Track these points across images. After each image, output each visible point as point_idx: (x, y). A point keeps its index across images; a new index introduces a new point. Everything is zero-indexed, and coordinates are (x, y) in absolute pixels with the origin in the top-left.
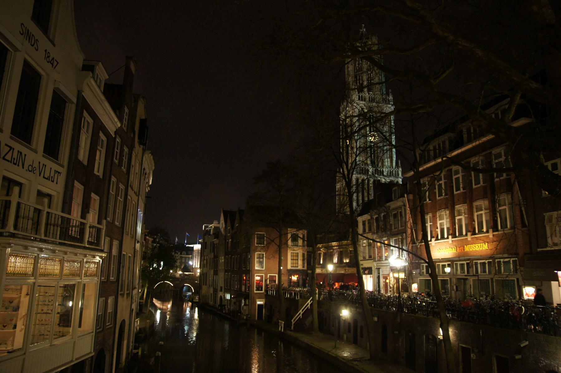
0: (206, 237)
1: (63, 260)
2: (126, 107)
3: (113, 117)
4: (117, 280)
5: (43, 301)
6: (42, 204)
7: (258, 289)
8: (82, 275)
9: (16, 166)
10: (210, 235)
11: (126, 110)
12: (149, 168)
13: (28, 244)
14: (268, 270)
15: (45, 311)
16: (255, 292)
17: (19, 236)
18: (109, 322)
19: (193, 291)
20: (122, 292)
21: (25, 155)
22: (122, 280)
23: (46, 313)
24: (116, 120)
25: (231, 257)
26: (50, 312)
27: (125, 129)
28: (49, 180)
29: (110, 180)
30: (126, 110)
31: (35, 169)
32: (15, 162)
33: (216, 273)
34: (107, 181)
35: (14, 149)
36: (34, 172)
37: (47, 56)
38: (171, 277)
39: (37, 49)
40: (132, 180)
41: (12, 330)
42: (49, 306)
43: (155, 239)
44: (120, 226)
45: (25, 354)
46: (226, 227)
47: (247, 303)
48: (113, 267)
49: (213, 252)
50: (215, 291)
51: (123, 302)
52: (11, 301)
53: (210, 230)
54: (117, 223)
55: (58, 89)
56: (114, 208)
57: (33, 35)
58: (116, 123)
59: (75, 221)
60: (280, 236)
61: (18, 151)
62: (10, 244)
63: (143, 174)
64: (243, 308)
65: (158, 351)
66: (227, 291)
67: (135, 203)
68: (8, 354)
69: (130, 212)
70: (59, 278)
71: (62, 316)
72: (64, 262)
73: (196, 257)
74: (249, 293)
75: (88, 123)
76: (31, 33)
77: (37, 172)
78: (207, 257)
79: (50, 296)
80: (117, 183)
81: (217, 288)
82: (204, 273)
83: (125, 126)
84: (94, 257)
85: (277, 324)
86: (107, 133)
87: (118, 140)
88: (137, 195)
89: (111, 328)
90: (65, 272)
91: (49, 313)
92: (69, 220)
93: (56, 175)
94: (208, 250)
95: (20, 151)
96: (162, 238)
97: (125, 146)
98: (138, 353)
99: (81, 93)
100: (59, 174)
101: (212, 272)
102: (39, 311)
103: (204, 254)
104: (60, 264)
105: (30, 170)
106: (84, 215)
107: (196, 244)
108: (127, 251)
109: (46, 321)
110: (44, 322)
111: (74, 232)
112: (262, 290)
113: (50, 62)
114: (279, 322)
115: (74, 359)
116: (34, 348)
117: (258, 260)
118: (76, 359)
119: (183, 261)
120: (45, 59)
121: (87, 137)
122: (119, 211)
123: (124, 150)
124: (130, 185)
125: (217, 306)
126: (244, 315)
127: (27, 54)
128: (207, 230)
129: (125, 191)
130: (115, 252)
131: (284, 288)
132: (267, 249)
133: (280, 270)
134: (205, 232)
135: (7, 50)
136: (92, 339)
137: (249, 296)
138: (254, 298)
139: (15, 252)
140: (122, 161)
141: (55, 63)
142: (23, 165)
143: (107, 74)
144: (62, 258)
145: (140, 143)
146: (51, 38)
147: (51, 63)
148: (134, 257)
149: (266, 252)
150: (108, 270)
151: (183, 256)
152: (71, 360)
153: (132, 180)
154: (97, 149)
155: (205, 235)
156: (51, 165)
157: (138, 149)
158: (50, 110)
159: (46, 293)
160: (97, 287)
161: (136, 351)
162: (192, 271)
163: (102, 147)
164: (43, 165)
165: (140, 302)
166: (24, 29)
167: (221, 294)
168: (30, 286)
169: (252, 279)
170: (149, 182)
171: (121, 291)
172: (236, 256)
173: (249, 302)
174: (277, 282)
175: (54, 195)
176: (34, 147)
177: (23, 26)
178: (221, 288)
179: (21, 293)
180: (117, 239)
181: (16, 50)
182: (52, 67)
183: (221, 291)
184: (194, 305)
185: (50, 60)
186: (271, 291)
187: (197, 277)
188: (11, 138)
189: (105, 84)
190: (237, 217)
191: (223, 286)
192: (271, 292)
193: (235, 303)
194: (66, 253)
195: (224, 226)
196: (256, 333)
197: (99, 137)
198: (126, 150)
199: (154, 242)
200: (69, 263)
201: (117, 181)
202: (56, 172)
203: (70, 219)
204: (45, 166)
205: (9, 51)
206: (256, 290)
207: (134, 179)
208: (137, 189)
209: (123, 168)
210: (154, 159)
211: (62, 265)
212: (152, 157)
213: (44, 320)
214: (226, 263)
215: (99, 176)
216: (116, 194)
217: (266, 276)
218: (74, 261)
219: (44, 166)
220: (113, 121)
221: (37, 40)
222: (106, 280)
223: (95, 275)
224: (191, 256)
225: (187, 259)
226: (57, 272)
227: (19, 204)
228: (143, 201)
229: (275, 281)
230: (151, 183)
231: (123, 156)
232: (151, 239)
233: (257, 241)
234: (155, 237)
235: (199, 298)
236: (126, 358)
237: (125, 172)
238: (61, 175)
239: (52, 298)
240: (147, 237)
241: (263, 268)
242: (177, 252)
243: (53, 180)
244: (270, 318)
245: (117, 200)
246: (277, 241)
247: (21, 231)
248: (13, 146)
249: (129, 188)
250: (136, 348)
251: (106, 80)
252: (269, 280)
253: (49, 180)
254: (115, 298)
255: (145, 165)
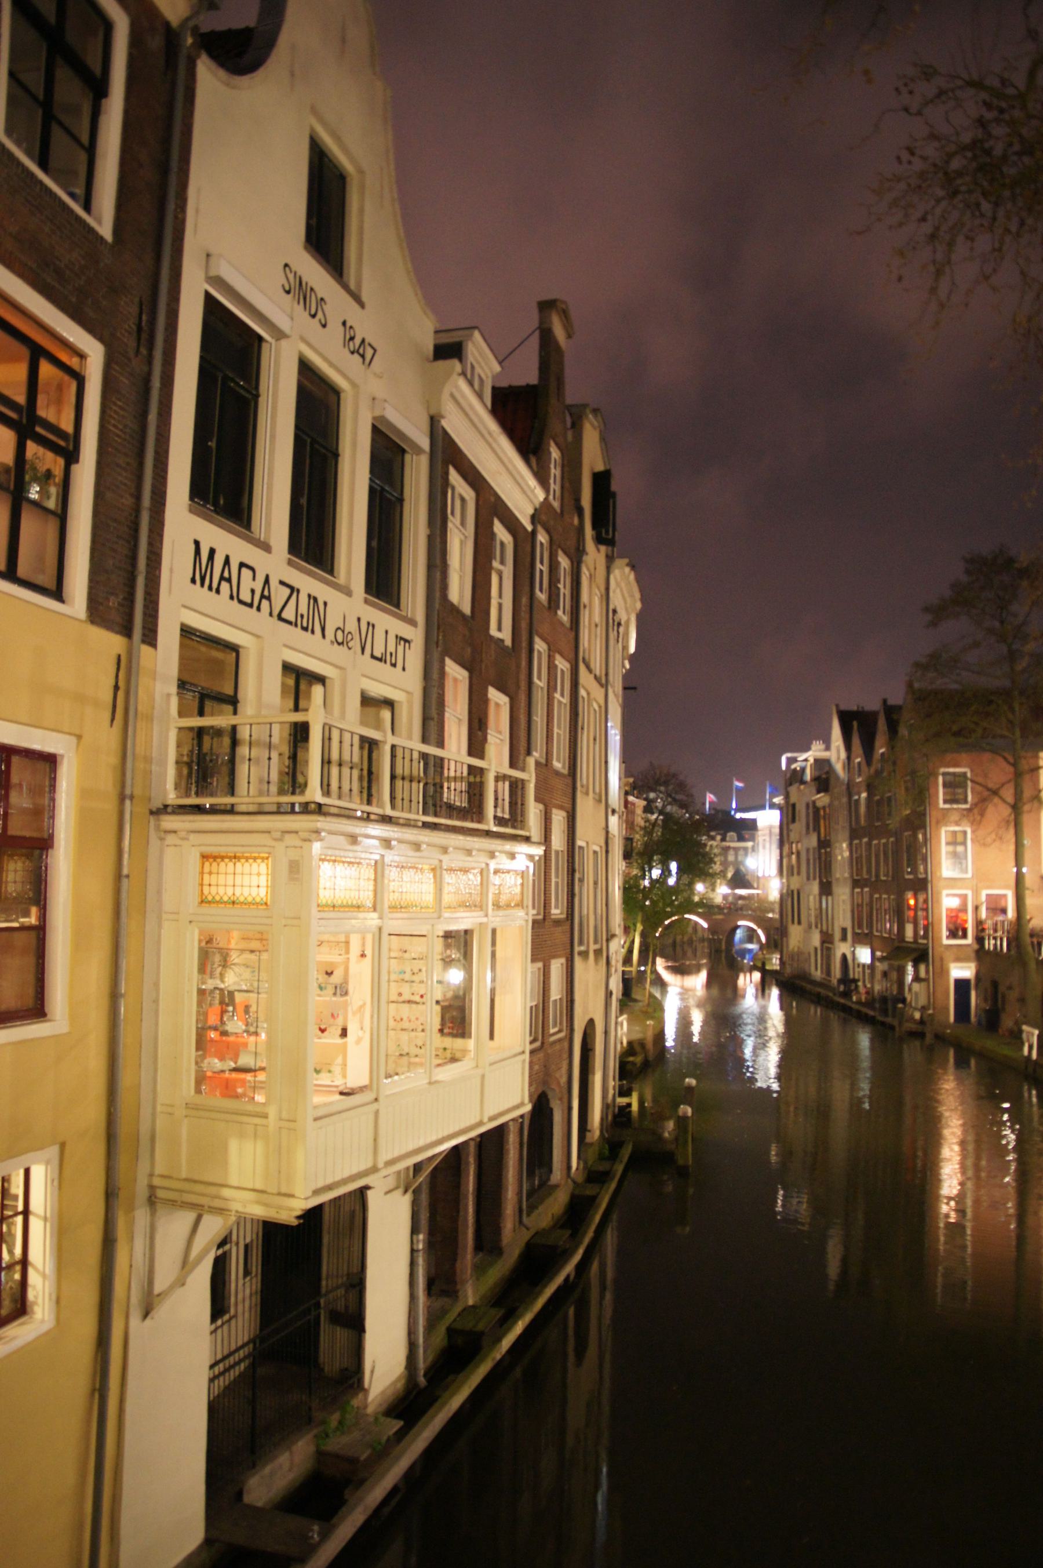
0: (793, 790)
1: (441, 867)
2: (552, 444)
3: (522, 477)
4: (567, 914)
5: (400, 973)
6: (378, 726)
7: (953, 934)
8: (487, 905)
9: (383, 664)
10: (802, 782)
11: (555, 454)
12: (626, 609)
13: (319, 825)
14: (981, 878)
15: (406, 996)
16: (946, 942)
17: (333, 810)
18: (555, 1026)
19: (763, 939)
20: (583, 948)
21: (325, 604)
22: (581, 917)
23: (409, 1002)
24: (532, 482)
25: (869, 844)
26: (417, 998)
27: (556, 505)
28: (385, 662)
29: (531, 650)
30: (555, 454)
31: (350, 637)
32: (305, 625)
33: (826, 889)
34: (524, 651)
35: (298, 591)
36: (350, 644)
37: (348, 337)
38: (700, 904)
39: (323, 322)
40: (586, 645)
41: (340, 1041)
42: (414, 984)
43: (650, 802)
44: (565, 771)
45: (376, 1100)
46: (849, 758)
47: (922, 974)
48: (558, 880)
49: (814, 830)
50: (827, 939)
51: (588, 974)
52: (329, 971)
53: (803, 769)
54: (557, 765)
55: (382, 419)
56: (548, 725)
57: (312, 289)
58: (533, 491)
59: (452, 764)
60: (1018, 775)
61: (309, 596)
62: (317, 832)
63: (614, 625)
64: (910, 990)
65: (684, 1103)
66: (860, 939)
67: (600, 707)
68: (343, 1097)
69: (588, 731)
70: (435, 915)
71: (445, 1010)
72: (441, 872)
73: (764, 847)
74: (927, 944)
75: (463, 500)
76: (307, 284)
77: (356, 644)
78: (799, 845)
79: (414, 959)
80: (549, 656)
81: (830, 932)
82: (792, 892)
83: (554, 498)
84: (512, 856)
85: (1017, 1037)
86: (512, 524)
87: (542, 537)
88: (602, 685)
89: (560, 1040)
90: (447, 899)
91: (417, 1003)
92: (440, 762)
93: (400, 648)
94: (798, 827)
95: (313, 594)
96: (670, 799)
97: (560, 552)
98: (629, 1105)
99: (439, 421)
100: (407, 645)
101: (815, 887)
102: (394, 997)
103: (788, 836)
104: (435, 876)
105: (340, 640)
106: (476, 746)
107: (762, 807)
108: (588, 837)
109: (410, 1021)
110: (406, 1024)
111: (454, 794)
112: (965, 936)
113: (358, 352)
114: (1021, 1031)
115: (485, 1120)
116: (390, 1086)
117: (951, 848)
118: (492, 1119)
119: (731, 858)
120: (344, 346)
121: (463, 537)
122: (561, 731)
123: (559, 563)
124: (584, 659)
125: (835, 982)
126: (916, 1009)
127: (303, 339)
128: (795, 769)
129: (572, 674)
130: (558, 841)
131: (1032, 930)
132: (978, 818)
133: (1019, 878)
134: (788, 775)
135: (260, 339)
136: (523, 1069)
137: (927, 954)
138: (942, 959)
139: (330, 852)
140: (558, 595)
141: (369, 353)
142: (323, 629)
143: (496, 358)
144: (436, 862)
145: (599, 540)
146: (352, 286)
147: (360, 354)
148: (607, 852)
149: (976, 824)
150: (545, 891)
151: (732, 845)
152: (477, 1120)
153: (586, 645)
154: (491, 568)
155: (791, 784)
156: (385, 622)
157: (594, 555)
158: (371, 479)
159: (406, 952)
160: (527, 937)
161: (622, 1101)
162: (755, 885)
163: (502, 562)
164: (369, 623)
165: (623, 972)
166: (291, 276)
167: (842, 948)
168: (369, 938)
169: (935, 905)
170: (625, 648)
171: (581, 943)
172: (884, 841)
173: (927, 972)
174: (1011, 914)
175: (399, 702)
176: (342, 580)
177: (287, 269)
178: (844, 931)
179: (347, 952)
180: (561, 808)
181: (280, 335)
182: (364, 363)
183: (844, 938)
184: (768, 979)
185: (357, 347)
186: (995, 938)
187: (773, 903)
188: (290, 563)
189: (494, 388)
190: (882, 725)
191: (848, 925)
192: (992, 942)
193: (885, 974)
194: (445, 850)
195: (843, 755)
196: (952, 1060)
197: (493, 535)
198: (564, 562)
199: (648, 809)
200: (453, 876)
201: (549, 650)
202: (400, 639)
203: (442, 759)
204: (373, 626)
205: (267, 341)
206: (948, 937)
207: (591, 641)
208: (601, 666)
209: (560, 613)
210: (638, 580)
211: (438, 880)
212: (632, 576)
213: (405, 1019)
214: (855, 861)
215: (502, 641)
216: (548, 685)
217: (976, 893)
218: (465, 871)
219: (371, 628)
220: (525, 487)
221: (322, 299)
222: (541, 917)
223: (520, 905)
224: (750, 844)
225: (741, 852)
226: (429, 898)
227: (327, 729)
228: (618, 701)
229: (1004, 911)
230: (632, 649)
231: (559, 581)
232: (640, 803)
233: (944, 794)
234: (652, 795)
235: (781, 959)
236: (602, 1119)
237: (568, 625)
238: (412, 645)
239: (420, 964)
240: (631, 798)
241: (966, 872)
242: (713, 833)
243: (393, 661)
244: (992, 1020)
245: (553, 702)
246: (1008, 794)
247: (402, 810)
248: (296, 585)
249: (582, 668)
250: (624, 1092)
251: (495, 377)
252: (987, 909)
253: (385, 662)
254: (567, 964)
255: (617, 600)
